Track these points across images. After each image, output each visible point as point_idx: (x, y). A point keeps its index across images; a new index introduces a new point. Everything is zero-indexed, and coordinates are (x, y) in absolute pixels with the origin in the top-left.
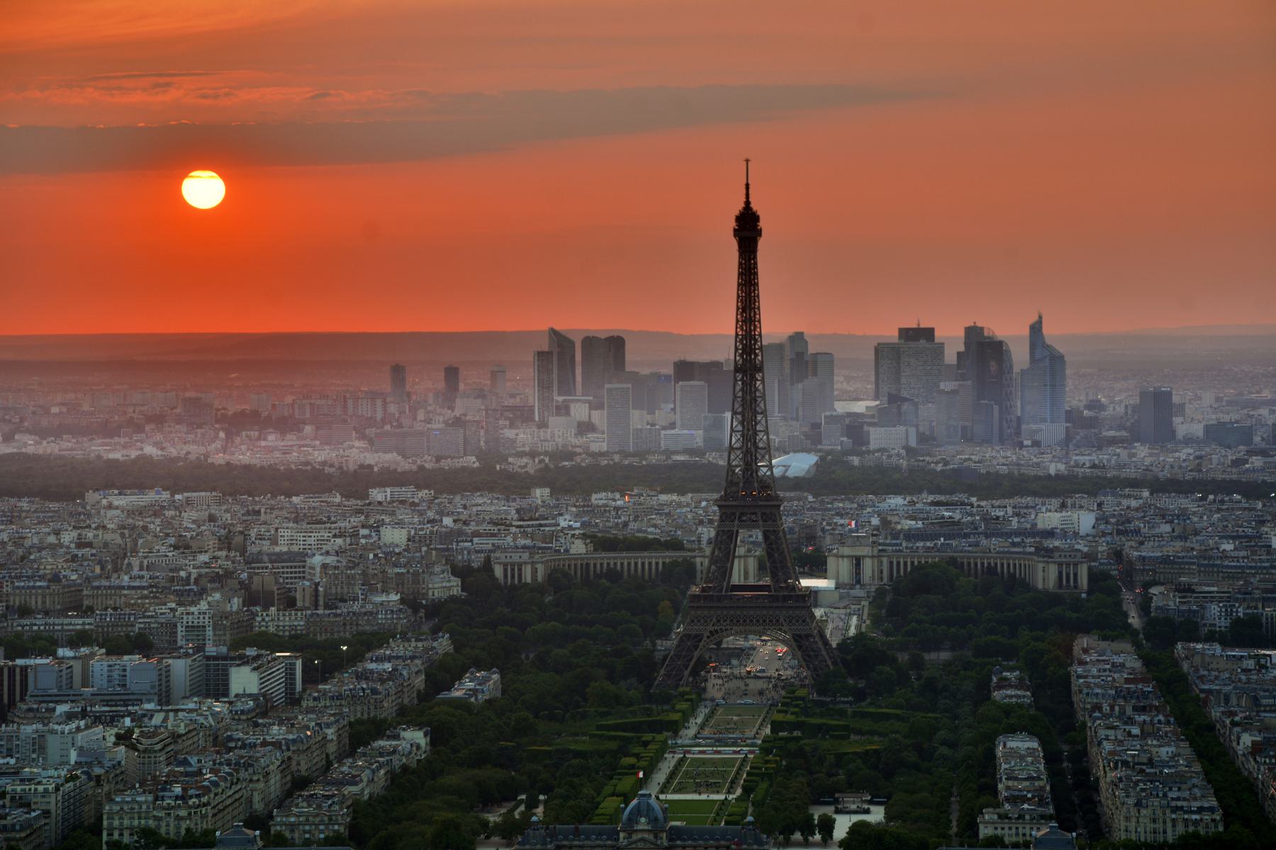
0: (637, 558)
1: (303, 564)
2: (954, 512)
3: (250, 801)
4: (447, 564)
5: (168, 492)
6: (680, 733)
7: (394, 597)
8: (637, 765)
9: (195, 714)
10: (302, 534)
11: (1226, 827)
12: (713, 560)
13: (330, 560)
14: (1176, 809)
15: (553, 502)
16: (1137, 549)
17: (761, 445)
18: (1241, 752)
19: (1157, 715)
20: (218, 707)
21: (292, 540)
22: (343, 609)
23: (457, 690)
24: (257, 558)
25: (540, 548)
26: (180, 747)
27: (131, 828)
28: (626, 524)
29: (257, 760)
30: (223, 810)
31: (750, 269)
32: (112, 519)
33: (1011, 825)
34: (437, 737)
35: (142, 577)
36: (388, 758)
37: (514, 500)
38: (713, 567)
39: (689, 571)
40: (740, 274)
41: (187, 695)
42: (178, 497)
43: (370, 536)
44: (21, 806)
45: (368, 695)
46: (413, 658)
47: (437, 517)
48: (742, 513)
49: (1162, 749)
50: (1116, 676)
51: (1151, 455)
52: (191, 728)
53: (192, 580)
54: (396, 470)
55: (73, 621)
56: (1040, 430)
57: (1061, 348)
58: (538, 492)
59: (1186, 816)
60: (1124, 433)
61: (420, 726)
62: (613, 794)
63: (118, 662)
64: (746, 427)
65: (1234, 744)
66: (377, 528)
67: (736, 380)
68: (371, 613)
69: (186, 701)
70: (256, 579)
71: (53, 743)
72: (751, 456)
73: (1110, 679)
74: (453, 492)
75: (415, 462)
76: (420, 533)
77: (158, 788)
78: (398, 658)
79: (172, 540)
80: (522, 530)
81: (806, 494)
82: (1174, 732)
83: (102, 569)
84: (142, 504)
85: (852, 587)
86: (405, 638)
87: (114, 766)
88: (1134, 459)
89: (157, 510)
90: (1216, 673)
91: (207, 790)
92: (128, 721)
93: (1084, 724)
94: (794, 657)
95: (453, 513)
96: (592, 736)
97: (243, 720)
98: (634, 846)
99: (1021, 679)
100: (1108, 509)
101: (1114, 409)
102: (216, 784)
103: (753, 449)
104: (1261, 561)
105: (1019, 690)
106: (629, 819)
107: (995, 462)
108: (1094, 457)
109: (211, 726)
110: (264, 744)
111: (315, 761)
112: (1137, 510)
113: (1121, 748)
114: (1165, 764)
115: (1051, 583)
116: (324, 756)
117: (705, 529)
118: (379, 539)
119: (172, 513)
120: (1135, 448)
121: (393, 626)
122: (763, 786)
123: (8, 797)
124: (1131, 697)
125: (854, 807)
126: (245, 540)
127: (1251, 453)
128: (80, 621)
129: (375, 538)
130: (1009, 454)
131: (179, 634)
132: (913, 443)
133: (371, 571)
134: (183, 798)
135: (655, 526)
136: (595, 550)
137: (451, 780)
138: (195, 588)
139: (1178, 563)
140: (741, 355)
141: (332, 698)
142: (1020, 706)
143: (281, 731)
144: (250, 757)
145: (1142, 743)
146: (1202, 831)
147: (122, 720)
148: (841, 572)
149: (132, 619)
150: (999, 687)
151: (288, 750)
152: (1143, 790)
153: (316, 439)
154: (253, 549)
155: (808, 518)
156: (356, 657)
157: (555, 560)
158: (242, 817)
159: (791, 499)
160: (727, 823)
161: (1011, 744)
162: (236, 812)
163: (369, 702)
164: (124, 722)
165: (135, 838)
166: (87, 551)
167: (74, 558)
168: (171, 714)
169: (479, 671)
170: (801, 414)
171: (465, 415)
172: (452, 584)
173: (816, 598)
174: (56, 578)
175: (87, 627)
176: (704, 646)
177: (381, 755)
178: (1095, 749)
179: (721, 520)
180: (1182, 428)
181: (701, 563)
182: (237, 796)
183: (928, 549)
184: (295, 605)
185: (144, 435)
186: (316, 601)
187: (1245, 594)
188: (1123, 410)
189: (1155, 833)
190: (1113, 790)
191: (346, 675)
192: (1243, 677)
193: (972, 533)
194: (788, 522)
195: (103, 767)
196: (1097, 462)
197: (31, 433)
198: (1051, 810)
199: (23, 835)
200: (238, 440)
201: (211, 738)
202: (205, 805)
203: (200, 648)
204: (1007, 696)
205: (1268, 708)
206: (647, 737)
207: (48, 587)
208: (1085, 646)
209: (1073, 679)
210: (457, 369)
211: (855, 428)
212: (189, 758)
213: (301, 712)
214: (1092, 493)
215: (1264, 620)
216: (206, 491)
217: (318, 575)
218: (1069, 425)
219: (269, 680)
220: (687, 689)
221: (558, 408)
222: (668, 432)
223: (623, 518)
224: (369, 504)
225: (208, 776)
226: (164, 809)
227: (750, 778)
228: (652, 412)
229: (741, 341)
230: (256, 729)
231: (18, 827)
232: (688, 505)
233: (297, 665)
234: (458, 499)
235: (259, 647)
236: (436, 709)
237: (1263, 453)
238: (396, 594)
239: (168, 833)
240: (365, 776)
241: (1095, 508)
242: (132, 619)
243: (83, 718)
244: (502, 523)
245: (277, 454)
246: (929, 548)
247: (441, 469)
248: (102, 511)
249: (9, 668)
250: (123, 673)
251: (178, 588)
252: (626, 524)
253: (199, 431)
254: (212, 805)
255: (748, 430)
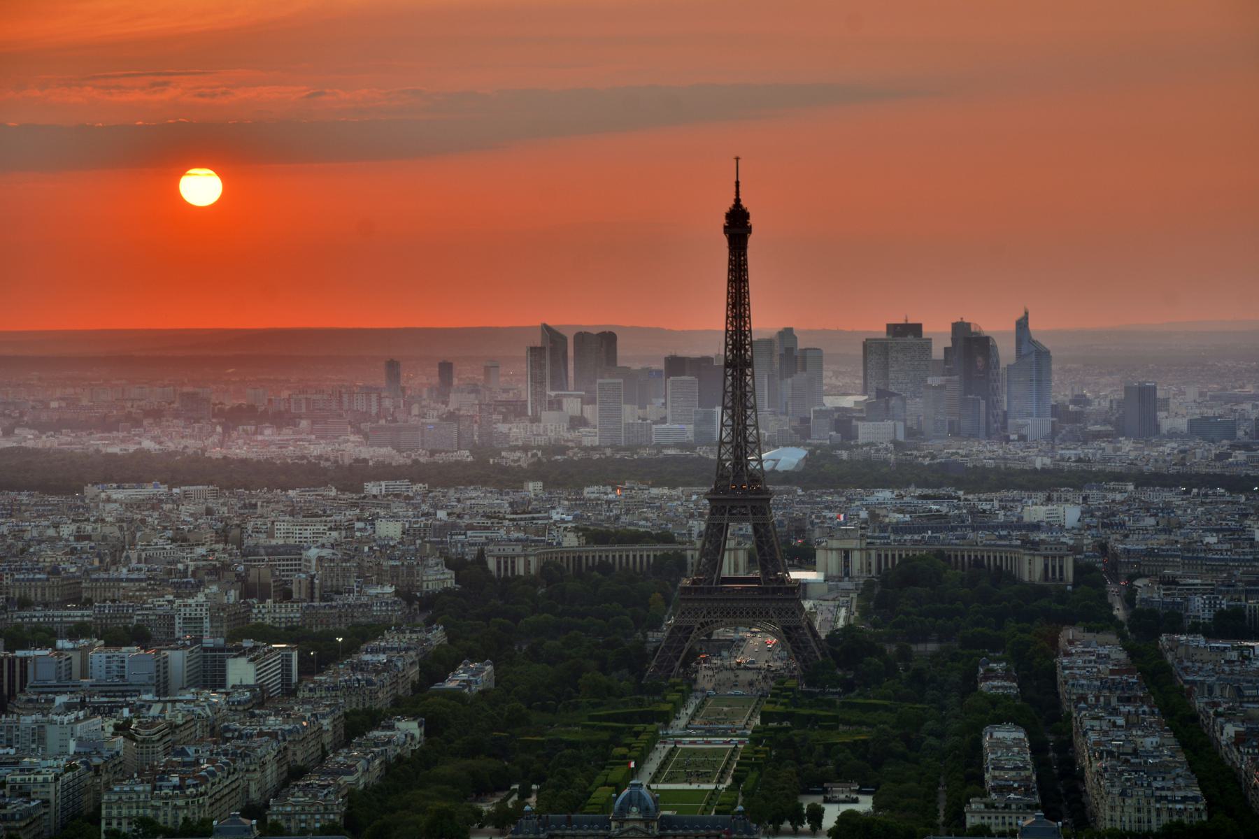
0: (628, 551)
1: (299, 556)
2: (941, 506)
3: (246, 791)
4: (441, 556)
5: (166, 486)
6: (671, 724)
7: (389, 589)
8: (629, 755)
9: (192, 705)
10: (297, 528)
11: (1210, 816)
12: (704, 553)
13: (326, 553)
14: (1160, 799)
15: (545, 496)
16: (1122, 542)
17: (751, 439)
18: (1225, 743)
19: (1142, 706)
20: (215, 698)
21: (288, 533)
22: (338, 601)
23: (451, 681)
24: (253, 551)
25: (533, 541)
26: (178, 737)
27: (129, 817)
28: (617, 518)
29: (254, 750)
30: (220, 799)
31: (740, 265)
32: (110, 512)
33: (997, 815)
34: (431, 727)
35: (141, 570)
36: (383, 748)
37: (508, 494)
38: (704, 560)
39: (680, 563)
40: (730, 271)
41: (185, 686)
42: (175, 490)
43: (365, 529)
44: (21, 795)
45: (363, 686)
46: (407, 649)
47: (431, 510)
48: (732, 507)
49: (1147, 739)
50: (1101, 667)
51: (1136, 449)
52: (189, 718)
53: (190, 573)
54: (390, 464)
55: (72, 613)
56: (1027, 425)
57: (1047, 344)
58: (531, 486)
59: (1170, 806)
60: (1109, 428)
61: (414, 717)
62: (605, 784)
63: (117, 653)
64: (736, 422)
65: (1218, 734)
66: (372, 521)
67: (726, 376)
68: (366, 605)
69: (183, 692)
70: (252, 571)
71: (52, 734)
72: (741, 450)
73: (1095, 670)
74: (447, 485)
75: (409, 456)
76: (415, 526)
77: (156, 777)
78: (392, 649)
79: (170, 533)
80: (515, 523)
81: (795, 488)
82: (1158, 723)
83: (101, 561)
84: (140, 497)
85: (841, 579)
86: (399, 630)
87: (112, 756)
88: (1119, 453)
89: (155, 504)
90: (1200, 665)
91: (204, 780)
92: (126, 712)
93: (1070, 714)
94: (783, 649)
95: (447, 506)
96: (584, 727)
97: (240, 711)
98: (626, 835)
99: (1007, 670)
100: (1093, 502)
101: (1099, 404)
102: (213, 774)
103: (743, 444)
104: (1244, 554)
105: (1005, 681)
106: (621, 809)
107: (982, 456)
108: (1079, 451)
109: (208, 717)
110: (261, 734)
111: (311, 751)
112: (1122, 503)
113: (1106, 739)
114: (1149, 754)
115: (1037, 576)
116: (320, 746)
117: (695, 523)
118: (374, 532)
119: (170, 506)
120: (1120, 442)
121: (387, 618)
122: (753, 775)
123: (8, 786)
124: (1116, 688)
125: (842, 796)
126: (242, 533)
127: (1234, 447)
128: (79, 613)
129: (370, 531)
130: (995, 448)
131: (177, 626)
132: (901, 437)
133: (366, 564)
134: (181, 787)
135: (646, 519)
136: (587, 543)
137: (445, 769)
138: (192, 580)
139: (1162, 556)
140: (731, 351)
141: (328, 689)
142: (1006, 697)
143: (278, 722)
144: (247, 747)
145: (1127, 733)
146: (1186, 821)
147: (120, 711)
148: (829, 565)
149: (130, 611)
150: (986, 678)
151: (285, 740)
152: (1127, 780)
153: (311, 433)
154: (249, 542)
155: (797, 512)
156: (351, 648)
157: (547, 553)
158: (239, 806)
159: (781, 493)
160: (717, 812)
161: (997, 735)
162: (233, 802)
163: (364, 693)
164: (122, 713)
165: (134, 827)
166: (86, 544)
167: (73, 551)
168: (169, 705)
169: (473, 663)
170: (790, 408)
171: (459, 410)
172: (446, 576)
173: (805, 590)
174: (55, 571)
175: (86, 619)
176: (695, 638)
177: (376, 745)
178: (1080, 739)
179: (712, 513)
180: (1167, 422)
181: (692, 555)
182: (234, 786)
183: (915, 542)
184: (291, 597)
185: (142, 430)
186: (312, 594)
187: (1229, 586)
188: (1108, 405)
189: (1139, 822)
190: (1098, 780)
191: (341, 666)
192: (1227, 669)
193: (959, 526)
194: (777, 515)
195: (101, 757)
196: (1082, 456)
197: (30, 428)
198: (1037, 800)
199: (23, 824)
200: (234, 434)
201: (209, 729)
202: (202, 794)
203: (197, 640)
204: (994, 687)
205: (1251, 699)
206: (639, 727)
207: (48, 580)
208: (1071, 638)
209: (1059, 670)
210: (451, 364)
211: (844, 422)
212: (187, 749)
213: (297, 703)
214: (1078, 487)
215: (1247, 612)
216: (203, 485)
217: (314, 568)
218: (1054, 419)
219: (265, 671)
220: (678, 680)
221: (550, 403)
222: (659, 426)
223: (615, 512)
224: (364, 498)
225: (205, 766)
226: (162, 798)
227: (740, 768)
228: (643, 407)
229: (731, 336)
230: (253, 720)
231: (17, 817)
232: (679, 499)
233: (293, 656)
234: (451, 492)
235: (256, 639)
236: (430, 700)
237: (1246, 447)
238: (391, 586)
239: (165, 823)
240: (361, 766)
241: (1081, 501)
242: (130, 611)
243: (82, 708)
244: (495, 516)
245: (274, 448)
246: (916, 540)
247: (435, 463)
248: (101, 505)
249: (9, 660)
250: (121, 665)
251: (176, 580)
252: (617, 518)
253: (196, 425)
254: (209, 795)
255: (738, 424)
